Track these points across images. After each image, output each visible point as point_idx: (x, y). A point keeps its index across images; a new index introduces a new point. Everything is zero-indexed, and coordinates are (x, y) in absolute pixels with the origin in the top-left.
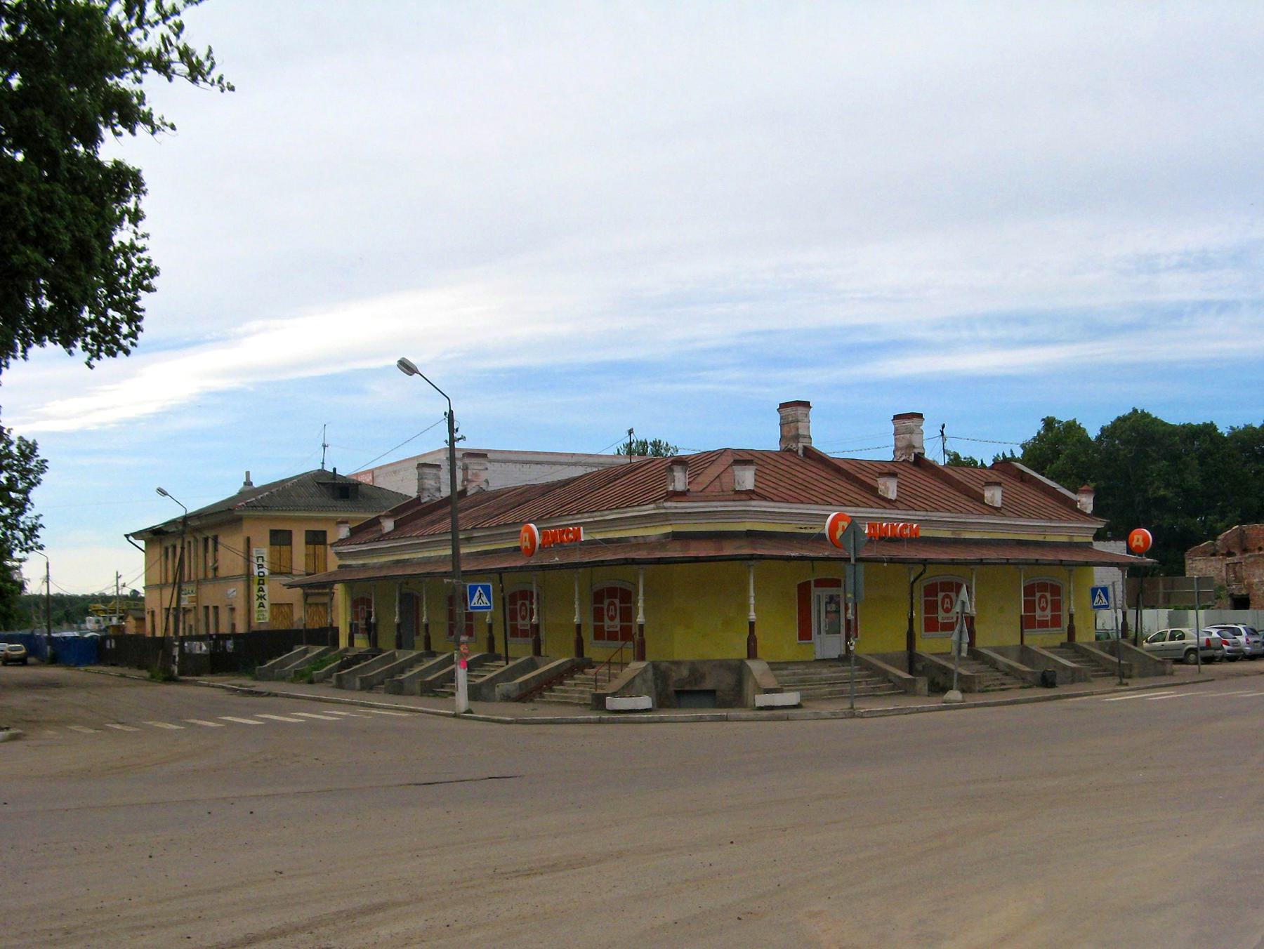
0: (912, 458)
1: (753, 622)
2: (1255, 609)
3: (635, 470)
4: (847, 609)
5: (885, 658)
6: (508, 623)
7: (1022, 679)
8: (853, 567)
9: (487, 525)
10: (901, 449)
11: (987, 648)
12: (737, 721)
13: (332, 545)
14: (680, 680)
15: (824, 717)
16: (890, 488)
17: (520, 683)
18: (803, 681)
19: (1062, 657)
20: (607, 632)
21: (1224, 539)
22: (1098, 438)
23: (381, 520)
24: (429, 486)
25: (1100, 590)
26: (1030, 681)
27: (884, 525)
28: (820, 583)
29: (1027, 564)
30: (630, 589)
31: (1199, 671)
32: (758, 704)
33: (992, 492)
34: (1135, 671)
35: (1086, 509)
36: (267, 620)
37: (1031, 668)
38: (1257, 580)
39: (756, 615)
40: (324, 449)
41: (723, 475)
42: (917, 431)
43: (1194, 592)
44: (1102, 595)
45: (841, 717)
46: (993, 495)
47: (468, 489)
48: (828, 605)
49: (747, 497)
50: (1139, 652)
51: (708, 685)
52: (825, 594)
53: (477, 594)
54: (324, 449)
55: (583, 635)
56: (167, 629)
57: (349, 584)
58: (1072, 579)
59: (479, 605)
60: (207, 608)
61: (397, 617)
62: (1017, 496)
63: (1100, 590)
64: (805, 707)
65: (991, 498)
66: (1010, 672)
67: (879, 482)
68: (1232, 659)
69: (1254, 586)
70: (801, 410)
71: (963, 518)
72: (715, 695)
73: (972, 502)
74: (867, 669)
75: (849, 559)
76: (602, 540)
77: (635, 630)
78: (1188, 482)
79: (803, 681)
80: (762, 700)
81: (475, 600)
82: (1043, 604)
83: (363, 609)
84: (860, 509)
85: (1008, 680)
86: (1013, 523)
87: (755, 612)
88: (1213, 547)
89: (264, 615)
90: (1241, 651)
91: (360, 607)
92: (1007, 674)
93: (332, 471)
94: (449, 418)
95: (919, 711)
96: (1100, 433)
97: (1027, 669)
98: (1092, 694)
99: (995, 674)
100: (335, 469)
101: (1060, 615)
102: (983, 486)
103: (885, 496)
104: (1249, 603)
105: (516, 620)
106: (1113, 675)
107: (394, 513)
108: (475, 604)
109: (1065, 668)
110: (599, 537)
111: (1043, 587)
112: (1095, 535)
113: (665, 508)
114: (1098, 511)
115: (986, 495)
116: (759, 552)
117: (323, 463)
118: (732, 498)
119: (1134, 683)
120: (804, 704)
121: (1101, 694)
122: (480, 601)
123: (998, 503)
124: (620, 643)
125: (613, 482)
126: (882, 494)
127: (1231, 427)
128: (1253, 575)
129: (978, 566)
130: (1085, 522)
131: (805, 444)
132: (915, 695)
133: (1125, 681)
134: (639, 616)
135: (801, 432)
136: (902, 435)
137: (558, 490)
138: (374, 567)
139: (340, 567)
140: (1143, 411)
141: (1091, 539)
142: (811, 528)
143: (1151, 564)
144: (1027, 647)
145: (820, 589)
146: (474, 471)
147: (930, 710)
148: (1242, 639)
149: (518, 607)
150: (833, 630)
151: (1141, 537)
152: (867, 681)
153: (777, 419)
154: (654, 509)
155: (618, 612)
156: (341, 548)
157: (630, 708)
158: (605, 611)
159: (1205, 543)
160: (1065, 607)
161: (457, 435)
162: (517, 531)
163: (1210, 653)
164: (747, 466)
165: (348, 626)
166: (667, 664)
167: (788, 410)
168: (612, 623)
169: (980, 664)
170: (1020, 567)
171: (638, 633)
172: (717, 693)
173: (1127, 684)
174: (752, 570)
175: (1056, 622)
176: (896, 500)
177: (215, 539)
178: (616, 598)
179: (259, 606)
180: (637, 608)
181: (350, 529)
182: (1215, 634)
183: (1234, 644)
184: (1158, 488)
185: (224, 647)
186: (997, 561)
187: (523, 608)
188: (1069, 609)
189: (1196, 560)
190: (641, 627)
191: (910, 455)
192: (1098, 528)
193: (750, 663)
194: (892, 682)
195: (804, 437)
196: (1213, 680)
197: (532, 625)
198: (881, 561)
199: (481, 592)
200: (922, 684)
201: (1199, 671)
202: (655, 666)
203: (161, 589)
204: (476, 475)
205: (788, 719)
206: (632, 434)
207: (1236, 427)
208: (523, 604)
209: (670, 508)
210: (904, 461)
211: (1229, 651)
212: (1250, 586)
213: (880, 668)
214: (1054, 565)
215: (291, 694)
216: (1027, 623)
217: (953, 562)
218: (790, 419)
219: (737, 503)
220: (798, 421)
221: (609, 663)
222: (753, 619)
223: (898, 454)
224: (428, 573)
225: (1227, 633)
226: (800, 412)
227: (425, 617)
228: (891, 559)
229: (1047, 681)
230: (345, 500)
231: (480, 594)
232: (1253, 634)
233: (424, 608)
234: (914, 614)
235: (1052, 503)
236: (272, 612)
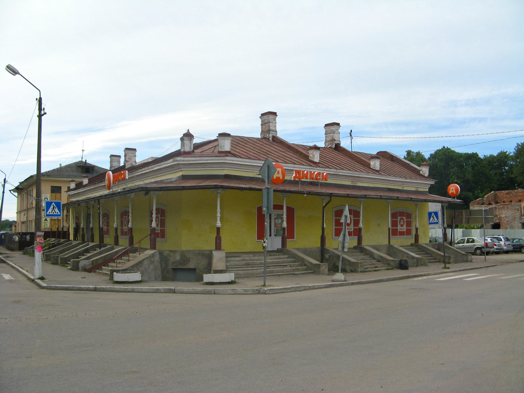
0: (334, 146)
2: (503, 229)
5: (306, 251)
7: (388, 264)
10: (328, 141)
11: (368, 246)
12: (181, 293)
14: (174, 262)
15: (239, 293)
17: (92, 261)
18: (248, 264)
19: (411, 251)
20: (399, 231)
21: (487, 197)
22: (429, 158)
24: (115, 166)
25: (433, 214)
26: (392, 266)
27: (305, 172)
29: (392, 199)
30: (164, 209)
31: (485, 260)
33: (374, 162)
34: (452, 260)
35: (425, 174)
36: (48, 227)
37: (393, 258)
38: (504, 216)
40: (83, 152)
42: (337, 132)
43: (483, 217)
44: (434, 216)
45: (250, 293)
46: (375, 163)
47: (126, 165)
48: (276, 220)
49: (225, 155)
50: (453, 249)
51: (191, 265)
53: (52, 207)
54: (83, 152)
56: (22, 231)
58: (417, 209)
59: (52, 214)
60: (30, 221)
62: (389, 167)
63: (433, 214)
64: (238, 283)
65: (374, 165)
66: (381, 260)
67: (310, 153)
68: (497, 253)
69: (502, 219)
70: (271, 117)
71: (356, 174)
72: (195, 270)
74: (293, 258)
78: (467, 177)
79: (248, 264)
81: (50, 210)
83: (125, 218)
84: (296, 166)
85: (379, 265)
86: (386, 178)
88: (482, 201)
89: (47, 224)
90: (502, 249)
92: (379, 261)
93: (85, 161)
94: (39, 101)
95: (310, 288)
96: (430, 157)
97: (391, 258)
98: (429, 275)
99: (372, 261)
100: (86, 160)
101: (411, 229)
102: (370, 159)
103: (313, 160)
104: (500, 226)
105: (123, 227)
106: (439, 262)
108: (49, 213)
109: (413, 258)
111: (402, 214)
112: (429, 187)
113: (177, 161)
114: (431, 175)
115: (371, 164)
117: (82, 158)
118: (217, 155)
119: (454, 267)
120: (237, 280)
121: (435, 274)
122: (53, 211)
123: (378, 168)
126: (311, 159)
127: (484, 155)
128: (502, 214)
130: (424, 180)
131: (273, 135)
132: (319, 274)
133: (447, 265)
135: (271, 128)
136: (329, 134)
140: (447, 147)
144: (392, 246)
146: (129, 157)
147: (319, 288)
148: (502, 243)
151: (454, 188)
152: (290, 265)
153: (259, 122)
154: (173, 162)
157: (124, 280)
159: (479, 199)
160: (413, 224)
163: (488, 250)
164: (226, 137)
166: (168, 252)
167: (265, 117)
168: (402, 228)
169: (364, 255)
170: (389, 201)
172: (197, 270)
173: (448, 268)
175: (409, 232)
176: (319, 163)
179: (45, 220)
181: (76, 184)
182: (489, 240)
183: (499, 245)
184: (454, 179)
185: (26, 238)
186: (374, 197)
187: (125, 220)
188: (416, 225)
189: (475, 207)
191: (333, 144)
193: (215, 253)
194: (307, 266)
195: (273, 131)
196: (496, 265)
198: (302, 193)
199: (55, 206)
200: (324, 267)
201: (485, 260)
202: (161, 253)
203: (20, 213)
204: (130, 159)
205: (215, 293)
207: (486, 155)
208: (125, 218)
209: (180, 161)
210: (330, 147)
211: (496, 249)
212: (500, 218)
213: (300, 257)
216: (394, 232)
218: (266, 122)
220: (269, 122)
222: (219, 226)
223: (327, 144)
225: (495, 240)
226: (271, 117)
227: (82, 225)
228: (310, 192)
229: (403, 266)
230: (87, 173)
231: (54, 207)
232: (507, 241)
233: (82, 220)
234: (325, 226)
235: (405, 170)
236: (51, 223)
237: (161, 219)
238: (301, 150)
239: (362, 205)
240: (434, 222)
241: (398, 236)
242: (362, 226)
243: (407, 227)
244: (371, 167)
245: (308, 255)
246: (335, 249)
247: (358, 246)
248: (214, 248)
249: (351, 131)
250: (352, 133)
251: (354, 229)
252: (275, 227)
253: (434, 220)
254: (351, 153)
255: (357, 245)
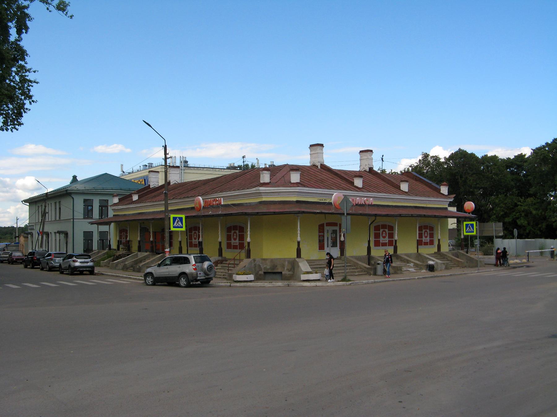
1: (300, 242)
3: (245, 174)
4: (340, 236)
6: (188, 241)
8: (345, 217)
9: (180, 197)
13: (110, 206)
16: (358, 182)
19: (437, 259)
20: (381, 243)
23: (132, 195)
28: (329, 224)
32: (302, 279)
39: (300, 239)
41: (285, 176)
44: (470, 227)
47: (171, 182)
48: (332, 234)
52: (330, 229)
55: (222, 246)
57: (118, 223)
61: (180, 238)
63: (470, 225)
73: (395, 189)
75: (344, 214)
76: (232, 204)
77: (246, 244)
80: (304, 277)
82: (426, 235)
83: (124, 234)
87: (300, 237)
91: (123, 233)
105: (231, 240)
107: (138, 192)
110: (230, 203)
116: (303, 210)
124: (239, 250)
125: (236, 179)
129: (398, 218)
134: (219, 239)
137: (211, 183)
138: (129, 215)
139: (114, 215)
141: (447, 206)
142: (325, 200)
143: (474, 217)
145: (328, 227)
149: (193, 234)
150: (334, 245)
155: (429, 235)
156: (114, 207)
158: (193, 236)
161: (168, 156)
162: (332, 194)
165: (117, 241)
171: (247, 246)
174: (299, 218)
175: (432, 243)
177: (60, 202)
178: (428, 229)
180: (395, 233)
187: (195, 234)
190: (249, 243)
192: (450, 201)
197: (199, 242)
206: (244, 158)
208: (195, 233)
214: (432, 217)
215: (446, 274)
217: (387, 216)
219: (292, 188)
221: (234, 259)
224: (153, 219)
231: (178, 221)
237: (239, 235)
238: (343, 175)
239: (397, 222)
240: (179, 226)
241: (423, 246)
242: (440, 238)
243: (389, 238)
244: (401, 189)
245: (360, 261)
246: (427, 254)
247: (394, 254)
248: (296, 257)
249: (383, 156)
250: (383, 157)
251: (389, 240)
252: (331, 240)
253: (470, 229)
254: (380, 174)
255: (393, 253)
